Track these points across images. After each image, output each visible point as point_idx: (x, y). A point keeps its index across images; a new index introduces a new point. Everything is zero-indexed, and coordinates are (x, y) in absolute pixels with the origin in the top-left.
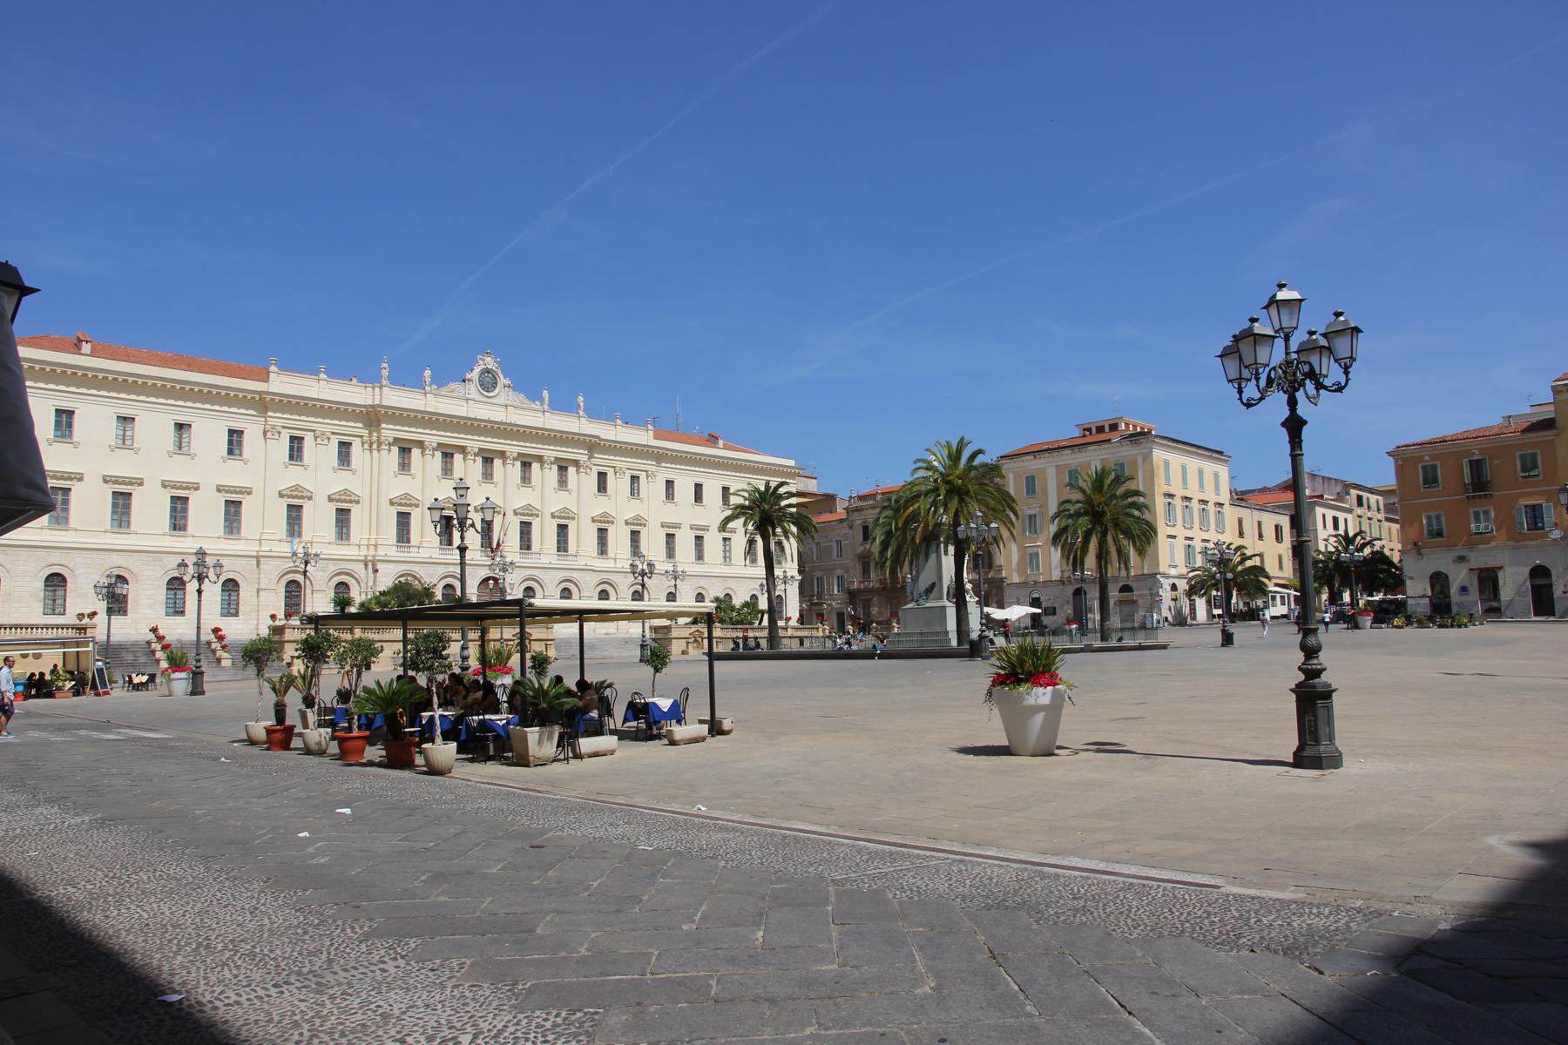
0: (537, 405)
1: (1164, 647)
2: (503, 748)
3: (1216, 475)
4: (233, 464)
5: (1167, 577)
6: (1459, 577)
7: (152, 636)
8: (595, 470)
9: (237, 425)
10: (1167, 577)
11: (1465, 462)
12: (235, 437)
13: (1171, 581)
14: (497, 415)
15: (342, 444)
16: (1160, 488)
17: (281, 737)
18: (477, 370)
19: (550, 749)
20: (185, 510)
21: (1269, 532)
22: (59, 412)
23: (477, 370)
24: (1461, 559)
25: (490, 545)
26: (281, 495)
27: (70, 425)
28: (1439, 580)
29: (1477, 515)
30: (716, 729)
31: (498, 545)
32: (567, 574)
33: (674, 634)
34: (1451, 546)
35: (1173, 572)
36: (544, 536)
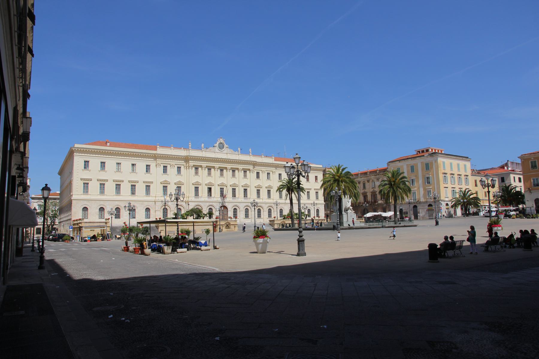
0: (237, 153)
1: (416, 226)
2: (159, 250)
3: (465, 166)
4: (148, 175)
7: (124, 225)
8: (256, 172)
9: (148, 164)
12: (148, 167)
13: (446, 202)
14: (224, 156)
15: (178, 167)
16: (441, 170)
17: (127, 249)
18: (218, 143)
19: (170, 251)
20: (135, 188)
21: (517, 180)
22: (101, 163)
23: (218, 143)
26: (161, 183)
27: (104, 166)
30: (215, 248)
33: (275, 222)
35: (447, 199)
36: (240, 192)
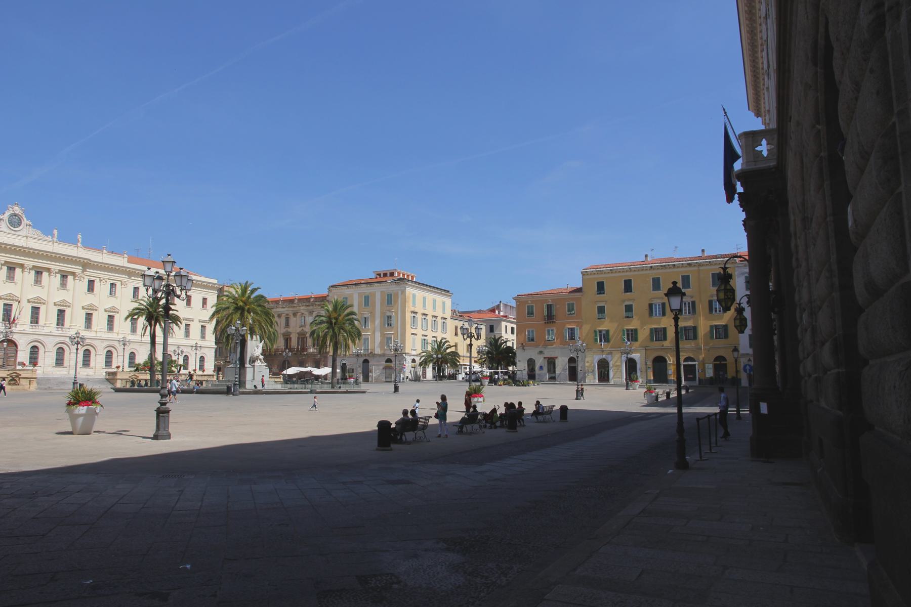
1: (364, 392)
3: (444, 303)
5: (410, 355)
6: (540, 361)
10: (410, 355)
11: (545, 305)
16: (409, 307)
18: (7, 214)
21: (509, 330)
23: (7, 214)
24: (541, 352)
25: (9, 320)
28: (531, 363)
29: (548, 331)
31: (14, 320)
32: (62, 339)
33: (119, 376)
34: (537, 346)
35: (414, 353)
